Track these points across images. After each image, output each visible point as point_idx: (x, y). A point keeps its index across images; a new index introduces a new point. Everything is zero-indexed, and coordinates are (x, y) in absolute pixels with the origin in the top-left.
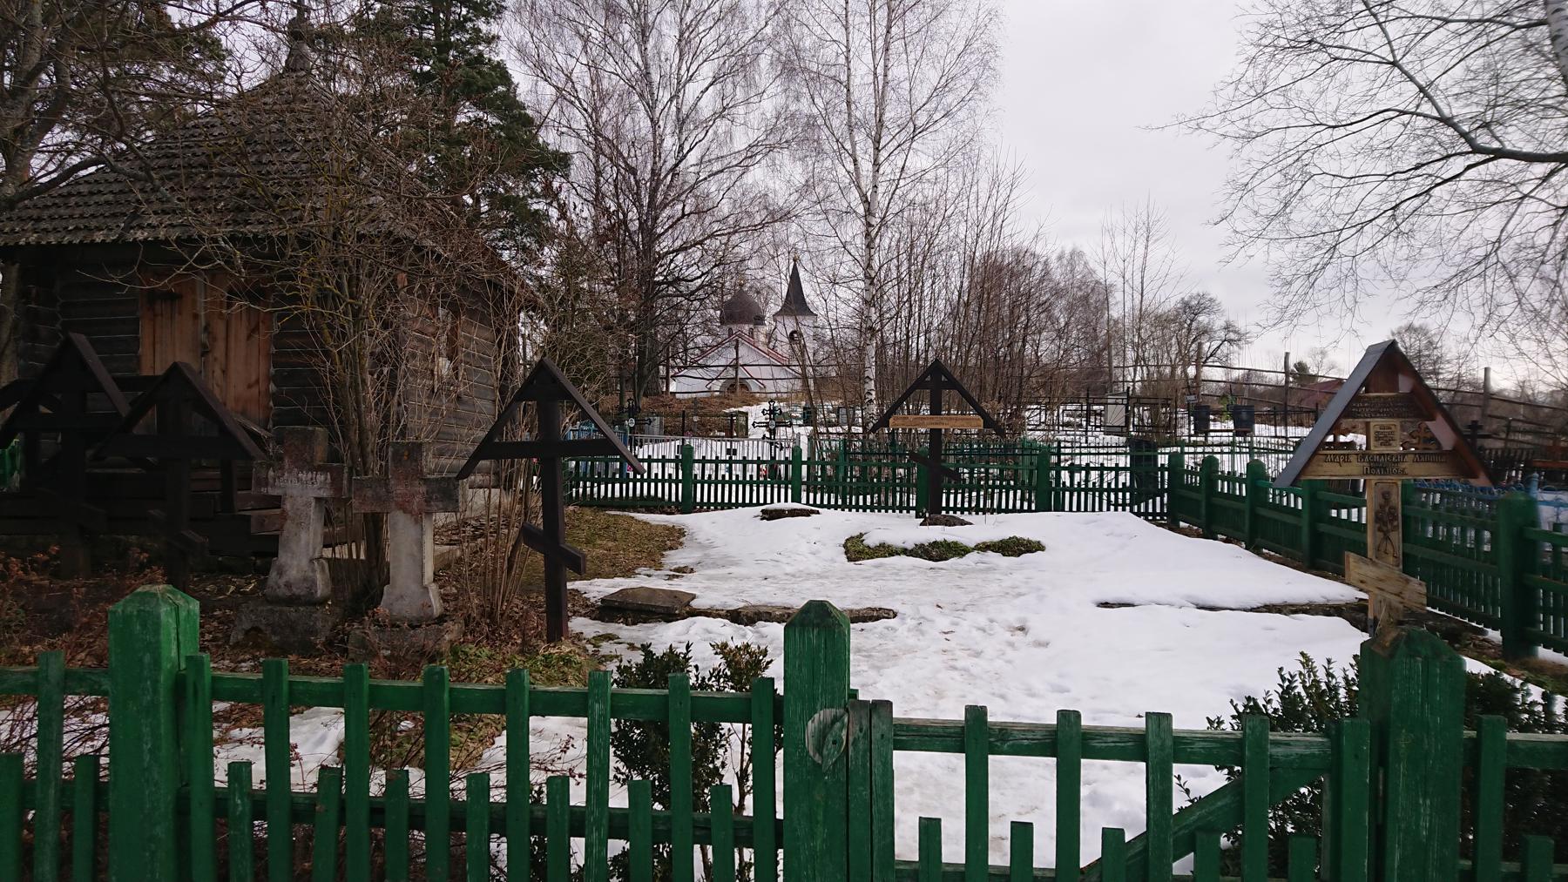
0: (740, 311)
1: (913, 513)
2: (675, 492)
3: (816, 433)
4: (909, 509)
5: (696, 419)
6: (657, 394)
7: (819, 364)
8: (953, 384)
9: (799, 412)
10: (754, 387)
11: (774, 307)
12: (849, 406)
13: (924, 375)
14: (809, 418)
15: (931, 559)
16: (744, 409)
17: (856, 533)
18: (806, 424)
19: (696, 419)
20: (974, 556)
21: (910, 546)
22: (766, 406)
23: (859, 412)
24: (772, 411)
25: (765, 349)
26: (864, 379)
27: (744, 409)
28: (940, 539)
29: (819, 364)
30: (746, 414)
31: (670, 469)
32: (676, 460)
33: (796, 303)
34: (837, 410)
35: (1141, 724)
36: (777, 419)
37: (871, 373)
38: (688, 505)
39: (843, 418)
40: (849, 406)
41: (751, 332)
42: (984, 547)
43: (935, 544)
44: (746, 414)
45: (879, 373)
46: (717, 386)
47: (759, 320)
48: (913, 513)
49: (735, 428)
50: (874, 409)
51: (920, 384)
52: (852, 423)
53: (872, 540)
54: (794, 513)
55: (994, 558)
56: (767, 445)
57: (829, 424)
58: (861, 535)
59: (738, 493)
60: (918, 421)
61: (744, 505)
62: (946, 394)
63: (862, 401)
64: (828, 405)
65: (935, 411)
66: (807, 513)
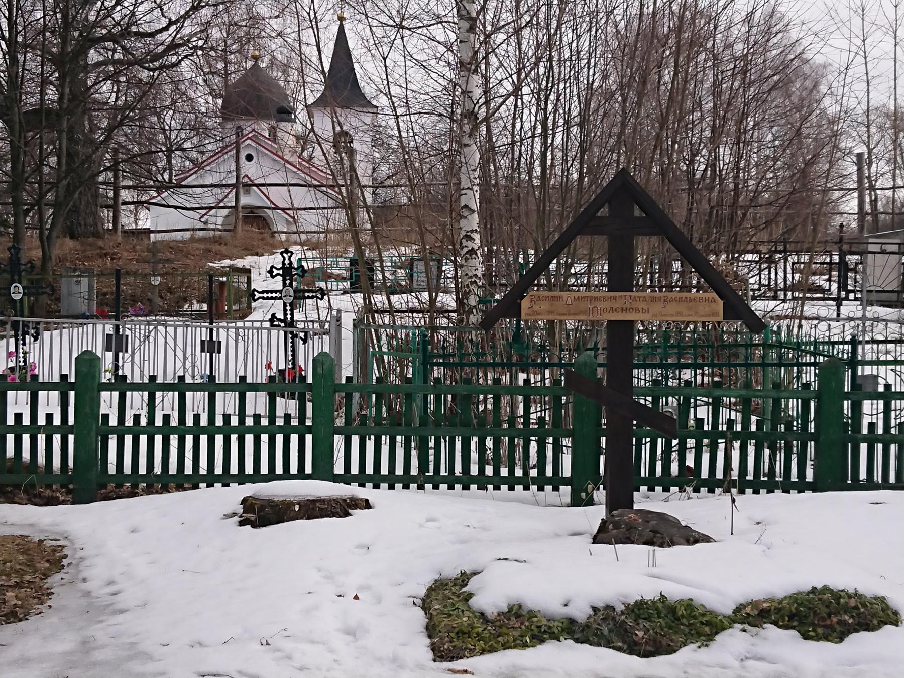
0: (253, 100)
1: (566, 490)
2: (59, 453)
3: (369, 309)
4: (557, 482)
5: (156, 281)
6: (97, 235)
7: (381, 185)
8: (658, 223)
9: (341, 266)
10: (280, 223)
11: (314, 91)
12: (432, 259)
13: (597, 205)
14: (361, 278)
15: (633, 648)
16: (246, 262)
17: (452, 572)
18: (354, 289)
19: (156, 281)
20: (733, 640)
21: (580, 612)
22: (277, 260)
23: (448, 269)
24: (287, 272)
25: (294, 159)
26: (458, 212)
27: (246, 262)
28: (649, 590)
29: (381, 185)
30: (247, 271)
31: (49, 402)
32: (63, 386)
33: (342, 86)
34: (410, 265)
35: (765, 625)
36: (300, 284)
37: (472, 199)
38: (89, 482)
39: (421, 279)
40: (432, 259)
41: (273, 131)
42: (757, 615)
43: (640, 609)
44: (247, 271)
45: (485, 199)
46: (218, 219)
47: (285, 113)
48: (566, 490)
49: (224, 301)
50: (477, 266)
51: (587, 223)
52: (435, 288)
53: (490, 596)
54: (314, 509)
55: (780, 642)
56: (278, 336)
57: (392, 290)
58: (464, 578)
59: (202, 454)
60: (578, 297)
61: (211, 480)
62: (644, 249)
63: (453, 245)
64: (390, 254)
65: (621, 279)
66: (342, 508)
